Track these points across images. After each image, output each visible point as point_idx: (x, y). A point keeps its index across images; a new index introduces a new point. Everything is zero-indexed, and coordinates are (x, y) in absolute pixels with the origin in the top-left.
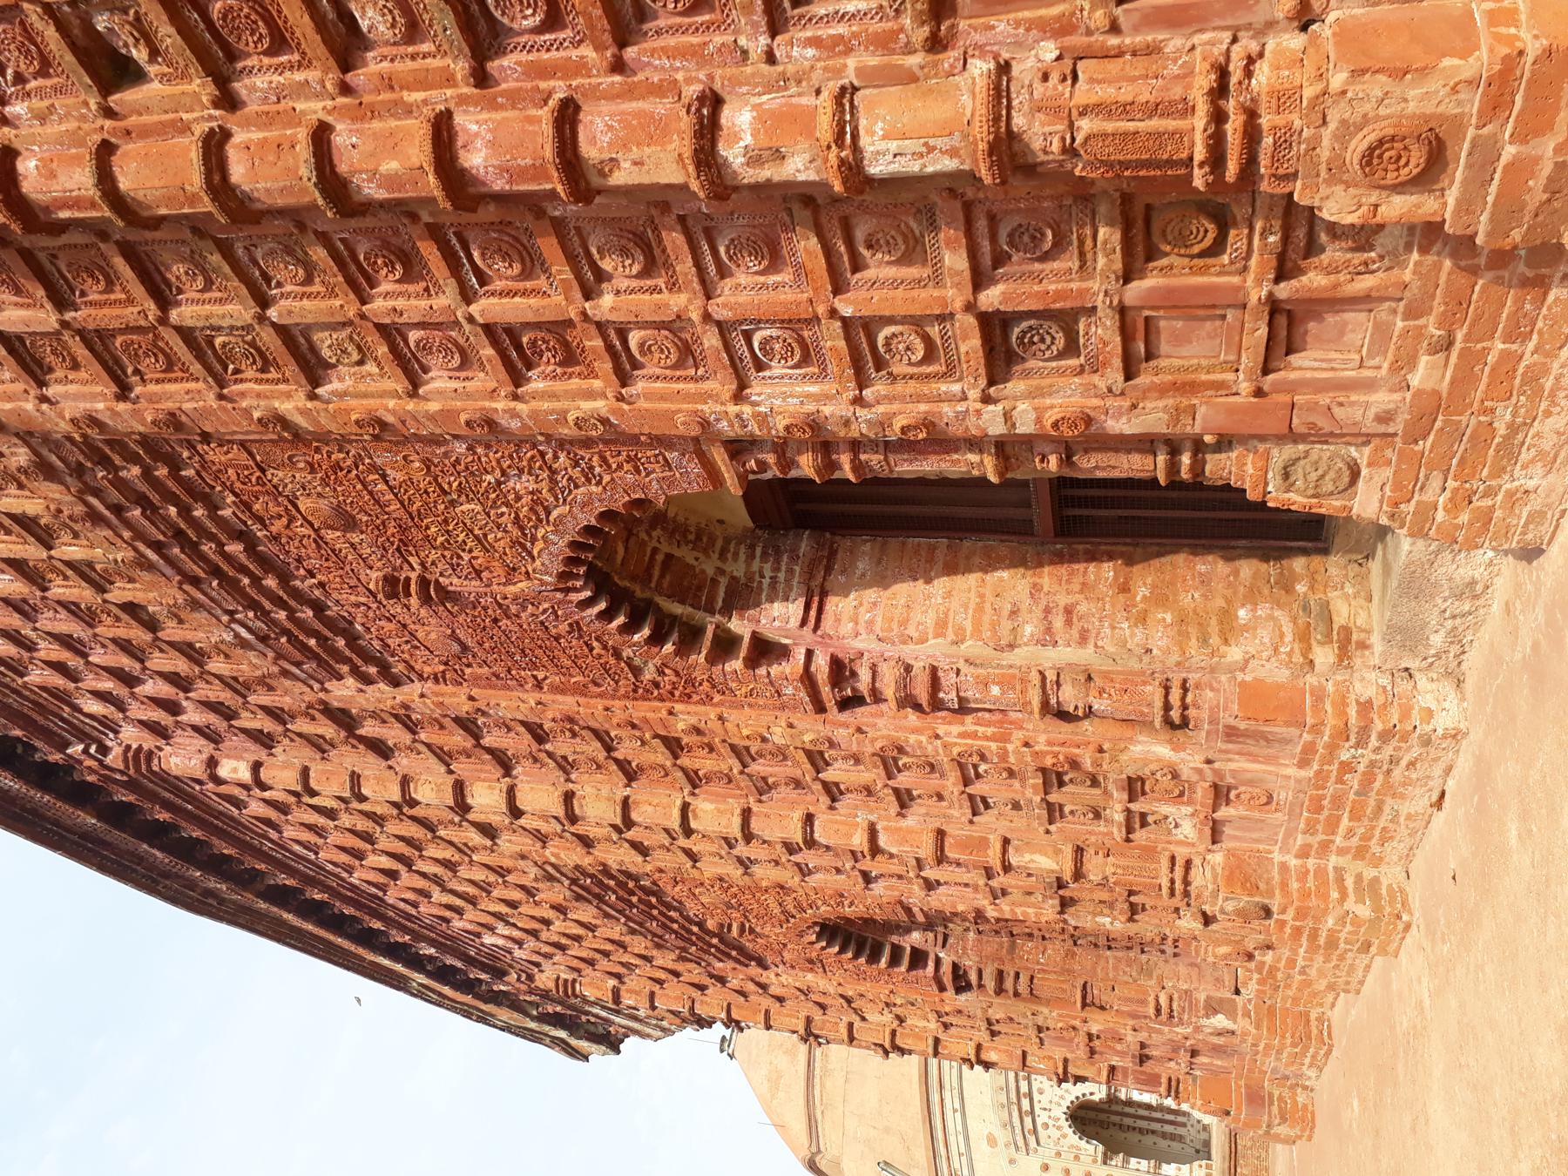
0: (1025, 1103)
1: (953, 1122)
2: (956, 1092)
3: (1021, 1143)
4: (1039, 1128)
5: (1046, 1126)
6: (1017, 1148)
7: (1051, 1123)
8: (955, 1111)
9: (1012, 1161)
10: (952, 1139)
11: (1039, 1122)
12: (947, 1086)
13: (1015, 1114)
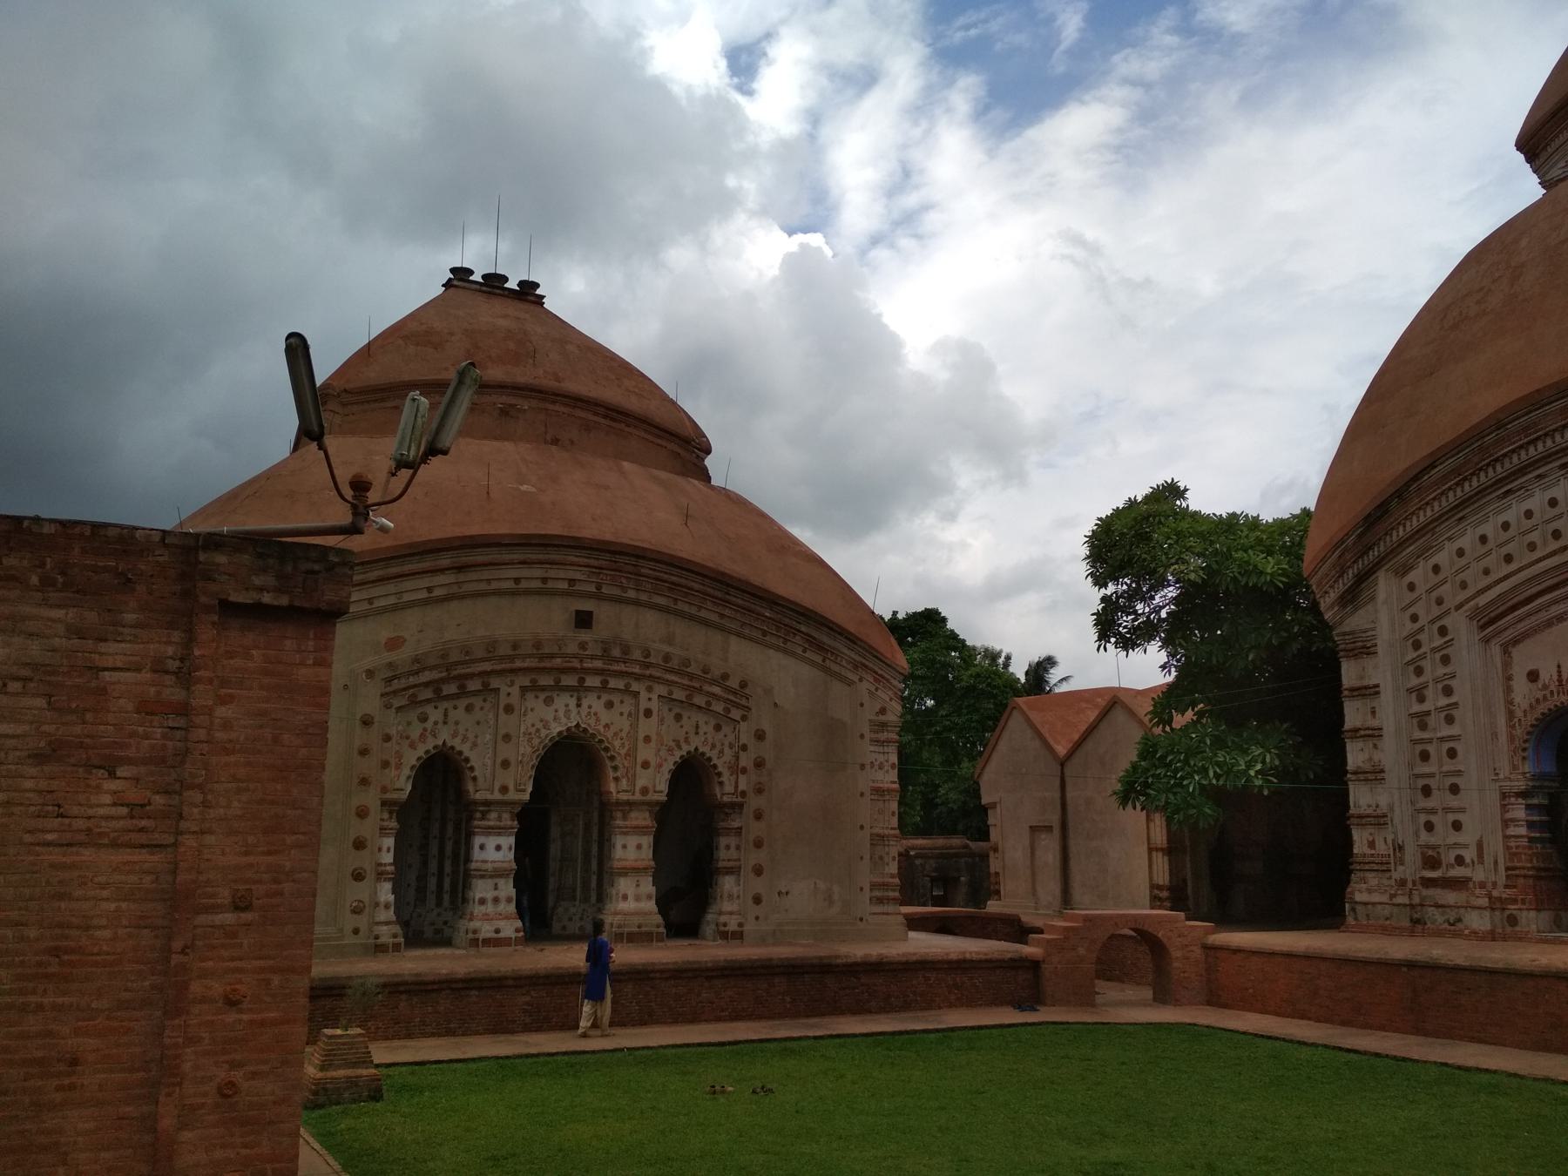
0: (451, 689)
1: (415, 589)
2: (455, 589)
3: (396, 685)
4: (420, 710)
5: (423, 719)
6: (389, 681)
7: (429, 725)
8: (430, 590)
9: (370, 673)
10: (391, 588)
11: (429, 709)
12: (462, 577)
13: (435, 675)
